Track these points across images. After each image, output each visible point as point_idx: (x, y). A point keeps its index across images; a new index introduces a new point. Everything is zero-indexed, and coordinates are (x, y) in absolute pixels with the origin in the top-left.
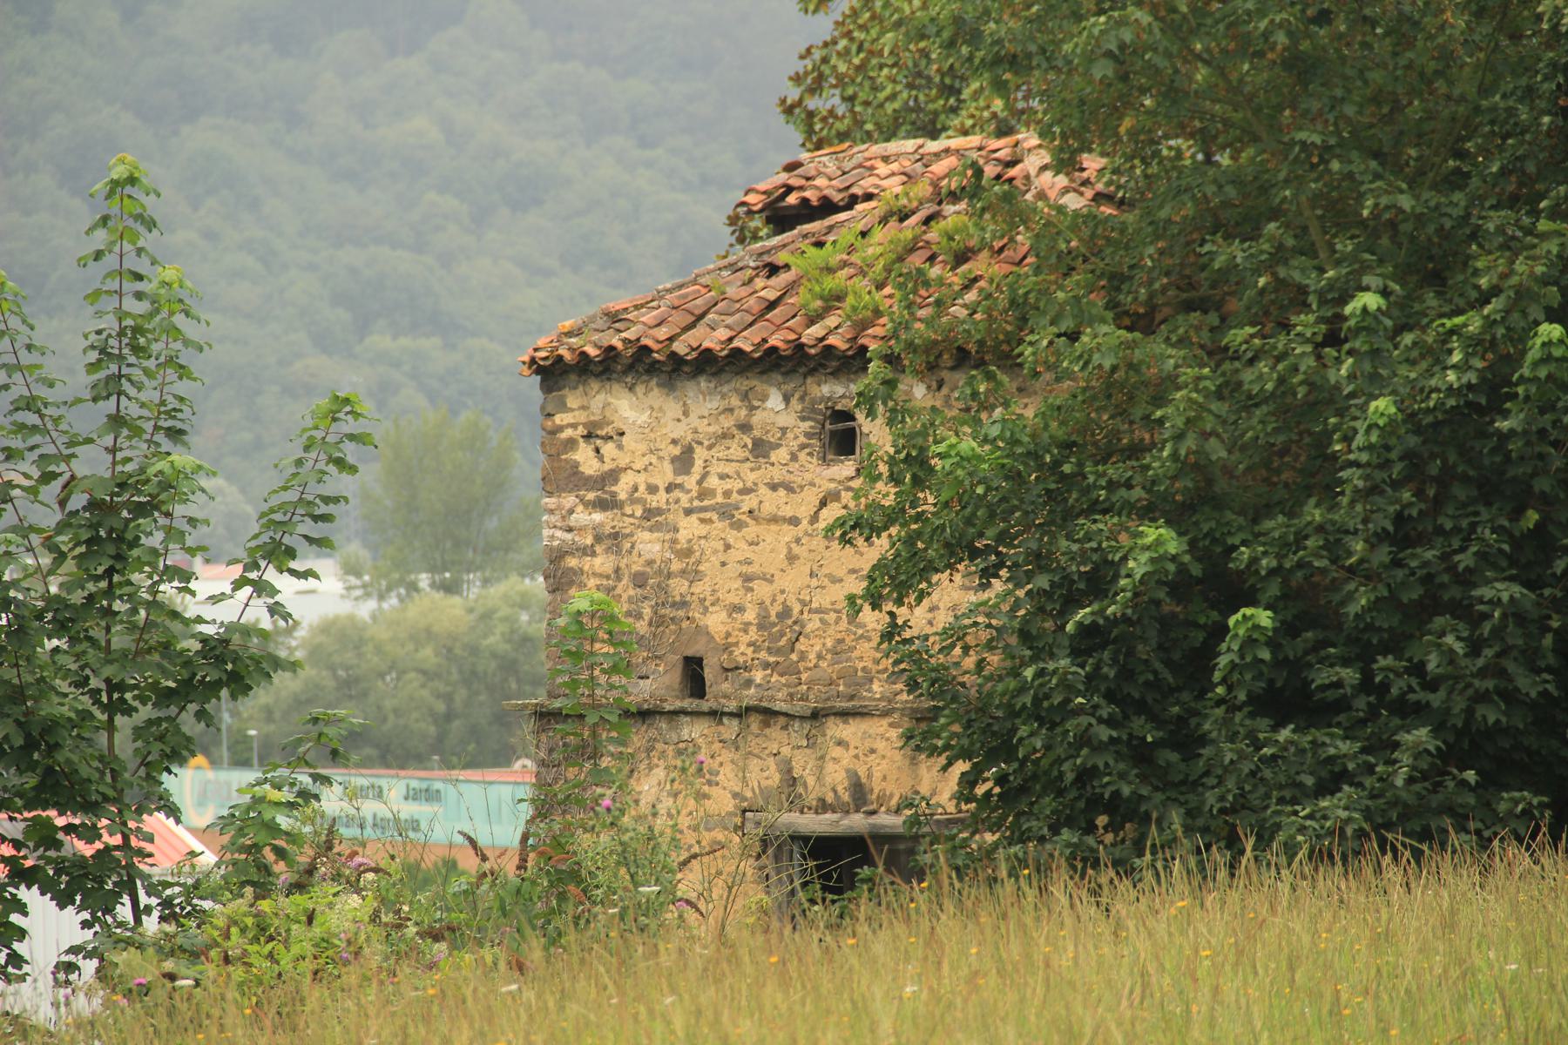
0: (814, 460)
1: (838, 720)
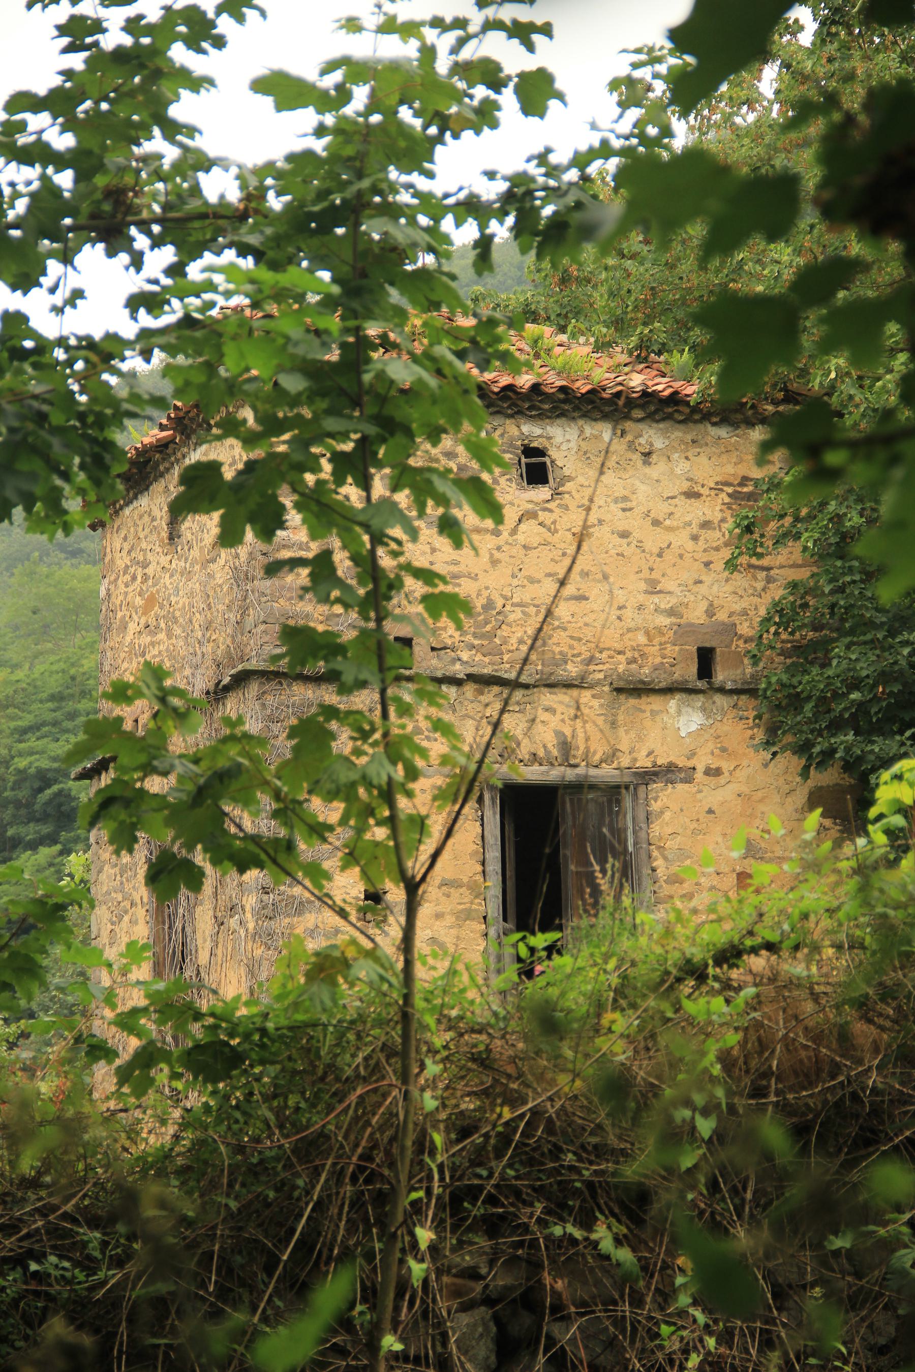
0: (514, 485)
1: (545, 690)
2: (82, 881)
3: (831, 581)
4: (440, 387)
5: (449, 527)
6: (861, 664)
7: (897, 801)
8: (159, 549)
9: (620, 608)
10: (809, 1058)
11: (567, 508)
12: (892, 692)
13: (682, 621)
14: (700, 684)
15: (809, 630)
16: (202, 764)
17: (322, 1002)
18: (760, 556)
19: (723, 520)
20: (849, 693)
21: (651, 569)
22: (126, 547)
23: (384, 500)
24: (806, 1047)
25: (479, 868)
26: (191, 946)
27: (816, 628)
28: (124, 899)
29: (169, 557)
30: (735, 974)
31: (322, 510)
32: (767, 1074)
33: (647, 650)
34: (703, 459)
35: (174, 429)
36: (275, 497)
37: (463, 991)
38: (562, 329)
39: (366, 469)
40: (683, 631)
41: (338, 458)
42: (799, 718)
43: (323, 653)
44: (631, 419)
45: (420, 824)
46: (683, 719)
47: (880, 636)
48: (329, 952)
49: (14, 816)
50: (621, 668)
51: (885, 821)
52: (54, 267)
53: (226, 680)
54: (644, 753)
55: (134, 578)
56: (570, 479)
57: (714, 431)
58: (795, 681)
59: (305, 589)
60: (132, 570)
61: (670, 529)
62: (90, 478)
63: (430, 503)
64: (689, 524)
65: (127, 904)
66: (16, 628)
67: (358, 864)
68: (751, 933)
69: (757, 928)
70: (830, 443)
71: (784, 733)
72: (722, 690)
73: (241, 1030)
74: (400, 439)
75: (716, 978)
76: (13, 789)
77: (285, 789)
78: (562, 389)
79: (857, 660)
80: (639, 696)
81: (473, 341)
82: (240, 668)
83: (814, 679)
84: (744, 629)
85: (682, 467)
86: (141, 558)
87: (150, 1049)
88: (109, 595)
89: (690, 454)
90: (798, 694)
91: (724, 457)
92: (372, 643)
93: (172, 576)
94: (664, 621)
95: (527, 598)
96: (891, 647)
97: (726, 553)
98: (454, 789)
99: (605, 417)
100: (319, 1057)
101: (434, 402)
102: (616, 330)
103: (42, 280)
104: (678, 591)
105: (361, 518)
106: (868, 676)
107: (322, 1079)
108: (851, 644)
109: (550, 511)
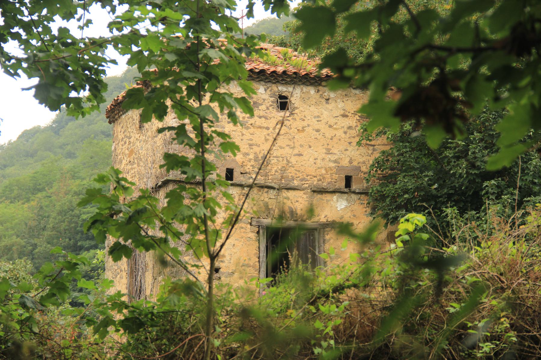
0: (275, 110)
2: (102, 261)
3: (398, 151)
4: (229, 61)
5: (232, 116)
6: (409, 184)
7: (407, 230)
8: (135, 132)
9: (315, 159)
10: (369, 330)
11: (295, 119)
12: (420, 195)
13: (340, 165)
14: (346, 190)
15: (387, 170)
16: (132, 207)
17: (174, 302)
18: (370, 140)
19: (357, 126)
20: (404, 195)
21: (328, 145)
22: (123, 130)
23: (208, 106)
24: (368, 326)
25: (257, 260)
26: (143, 287)
27: (392, 169)
28: (118, 269)
29: (139, 135)
30: (341, 296)
31: (182, 109)
32: (352, 336)
33: (325, 176)
34: (349, 102)
35: (142, 85)
36: (164, 103)
37: (232, 300)
38: (296, 50)
39: (200, 92)
40: (340, 169)
41: (189, 88)
42: (384, 204)
43: (180, 165)
44: (321, 86)
45: (217, 233)
46: (339, 203)
47: (416, 173)
48: (177, 282)
49: (81, 237)
50: (315, 183)
51: (401, 237)
52: (80, 11)
53: (160, 183)
54: (323, 216)
55: (125, 143)
56: (297, 108)
57: (354, 91)
58: (383, 190)
59: (174, 139)
60: (125, 140)
61: (336, 129)
62: (92, 94)
63: (225, 107)
64: (343, 127)
65: (119, 271)
66: (84, 164)
67: (192, 249)
68: (348, 280)
69: (350, 278)
70: (346, 67)
71: (378, 210)
72: (354, 192)
73: (143, 313)
74: (214, 81)
75: (333, 297)
76: (81, 227)
77: (165, 218)
78: (295, 73)
79: (407, 182)
80: (322, 194)
81: (245, 45)
82: (165, 179)
83: (390, 189)
84: (364, 169)
85: (341, 105)
86: (128, 135)
87: (107, 319)
88: (115, 149)
89: (344, 100)
90: (384, 195)
91: (358, 101)
92: (200, 161)
93: (140, 142)
94: (332, 165)
95: (279, 155)
96: (421, 177)
97: (357, 139)
98: (230, 220)
99: (312, 84)
100: (174, 324)
101: (227, 67)
102: (317, 51)
103: (75, 16)
104: (338, 153)
105: (196, 111)
106: (411, 188)
107: (175, 333)
108: (405, 175)
109: (289, 120)
